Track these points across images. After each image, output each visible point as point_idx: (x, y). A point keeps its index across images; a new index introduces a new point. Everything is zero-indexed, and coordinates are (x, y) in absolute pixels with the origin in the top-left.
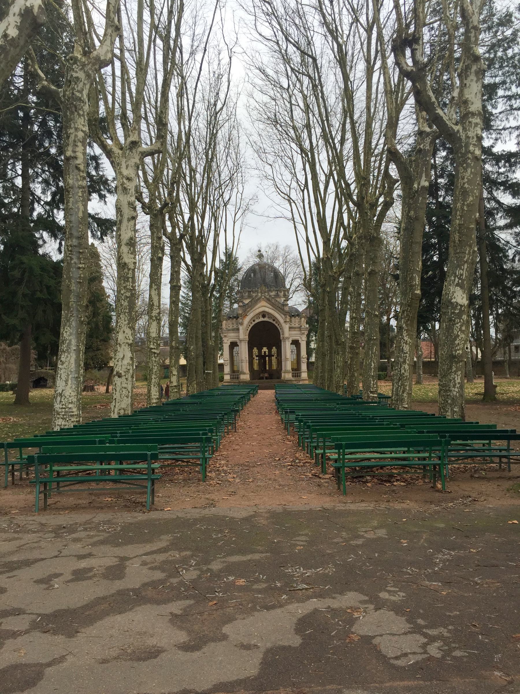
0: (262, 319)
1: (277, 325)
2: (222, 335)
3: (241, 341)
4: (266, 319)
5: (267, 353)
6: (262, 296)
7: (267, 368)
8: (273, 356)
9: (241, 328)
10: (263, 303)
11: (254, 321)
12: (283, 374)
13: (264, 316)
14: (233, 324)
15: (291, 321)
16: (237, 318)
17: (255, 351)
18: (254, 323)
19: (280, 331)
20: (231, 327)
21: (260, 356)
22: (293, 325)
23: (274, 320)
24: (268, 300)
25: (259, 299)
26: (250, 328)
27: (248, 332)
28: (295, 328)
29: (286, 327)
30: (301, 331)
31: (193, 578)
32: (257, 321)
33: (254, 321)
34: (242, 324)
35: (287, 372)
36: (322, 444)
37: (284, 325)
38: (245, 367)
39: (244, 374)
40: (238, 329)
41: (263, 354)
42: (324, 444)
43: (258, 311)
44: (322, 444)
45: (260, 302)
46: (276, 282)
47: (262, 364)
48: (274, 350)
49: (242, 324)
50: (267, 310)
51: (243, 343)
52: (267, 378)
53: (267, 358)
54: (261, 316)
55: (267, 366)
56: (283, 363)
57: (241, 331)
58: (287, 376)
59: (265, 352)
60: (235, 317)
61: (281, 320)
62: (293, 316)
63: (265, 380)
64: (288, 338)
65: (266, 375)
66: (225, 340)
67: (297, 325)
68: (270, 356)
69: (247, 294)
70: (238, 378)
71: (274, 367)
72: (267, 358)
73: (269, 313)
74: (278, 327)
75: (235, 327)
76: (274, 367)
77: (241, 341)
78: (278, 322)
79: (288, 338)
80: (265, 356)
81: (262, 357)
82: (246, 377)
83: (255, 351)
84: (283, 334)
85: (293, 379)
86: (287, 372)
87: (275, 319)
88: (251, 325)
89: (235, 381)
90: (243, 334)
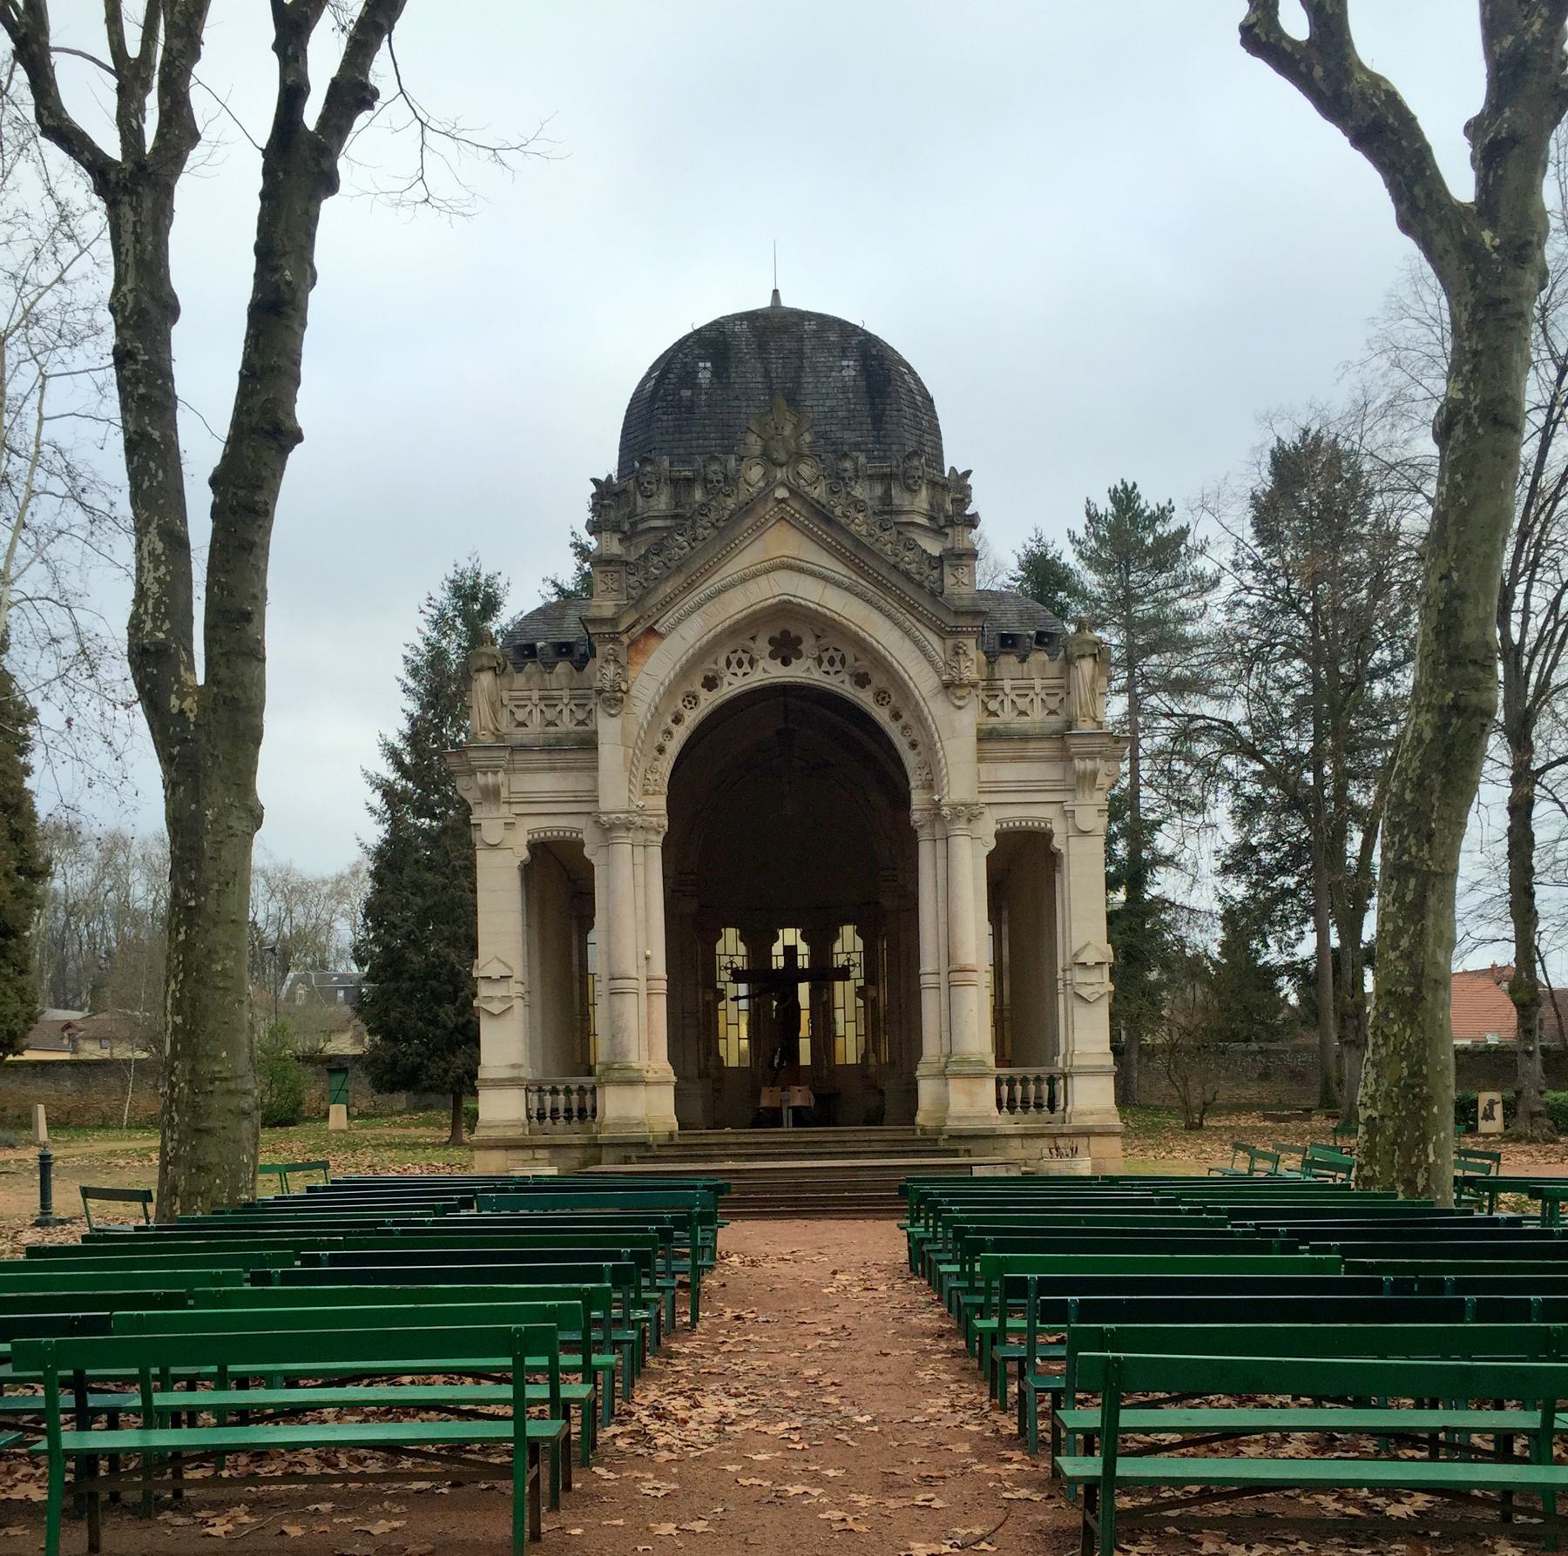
0: (769, 672)
1: (881, 715)
2: (466, 788)
3: (608, 830)
4: (801, 672)
5: (803, 962)
6: (770, 485)
7: (805, 1059)
8: (844, 974)
9: (608, 729)
10: (782, 542)
11: (711, 683)
12: (927, 1090)
13: (786, 649)
14: (549, 701)
15: (991, 687)
16: (575, 654)
17: (731, 947)
18: (709, 701)
19: (910, 759)
20: (535, 728)
21: (759, 976)
22: (1007, 717)
23: (862, 680)
24: (822, 521)
25: (746, 509)
26: (681, 733)
27: (666, 765)
28: (1025, 737)
29: (955, 729)
30: (1066, 757)
31: (1055, 842)
32: (734, 684)
33: (711, 683)
34: (615, 699)
35: (954, 1069)
36: (543, 1392)
37: (937, 709)
38: (637, 1025)
39: (633, 1081)
40: (588, 744)
41: (779, 963)
42: (519, 1392)
43: (738, 604)
44: (532, 1392)
45: (760, 529)
46: (878, 421)
47: (774, 1030)
48: (848, 944)
49: (615, 699)
50: (810, 593)
51: (623, 849)
52: (801, 1118)
53: (804, 989)
54: (762, 646)
55: (805, 1046)
56: (930, 1005)
57: (611, 754)
58: (959, 1098)
59: (790, 952)
60: (563, 650)
61: (921, 677)
62: (1009, 642)
63: (787, 1132)
64: (971, 813)
65: (800, 1097)
66: (489, 824)
67: (1037, 717)
68: (824, 974)
69: (662, 502)
70: (585, 1114)
71: (849, 1046)
72: (804, 989)
73: (825, 626)
74: (893, 729)
75: (567, 725)
76: (849, 1046)
77: (608, 830)
78: (894, 689)
79: (971, 813)
80: (792, 974)
81: (772, 987)
82: (645, 1104)
83: (731, 947)
84: (930, 786)
85: (1003, 1122)
86: (954, 1069)
87: (870, 666)
88: (692, 718)
89: (563, 1133)
90: (629, 780)
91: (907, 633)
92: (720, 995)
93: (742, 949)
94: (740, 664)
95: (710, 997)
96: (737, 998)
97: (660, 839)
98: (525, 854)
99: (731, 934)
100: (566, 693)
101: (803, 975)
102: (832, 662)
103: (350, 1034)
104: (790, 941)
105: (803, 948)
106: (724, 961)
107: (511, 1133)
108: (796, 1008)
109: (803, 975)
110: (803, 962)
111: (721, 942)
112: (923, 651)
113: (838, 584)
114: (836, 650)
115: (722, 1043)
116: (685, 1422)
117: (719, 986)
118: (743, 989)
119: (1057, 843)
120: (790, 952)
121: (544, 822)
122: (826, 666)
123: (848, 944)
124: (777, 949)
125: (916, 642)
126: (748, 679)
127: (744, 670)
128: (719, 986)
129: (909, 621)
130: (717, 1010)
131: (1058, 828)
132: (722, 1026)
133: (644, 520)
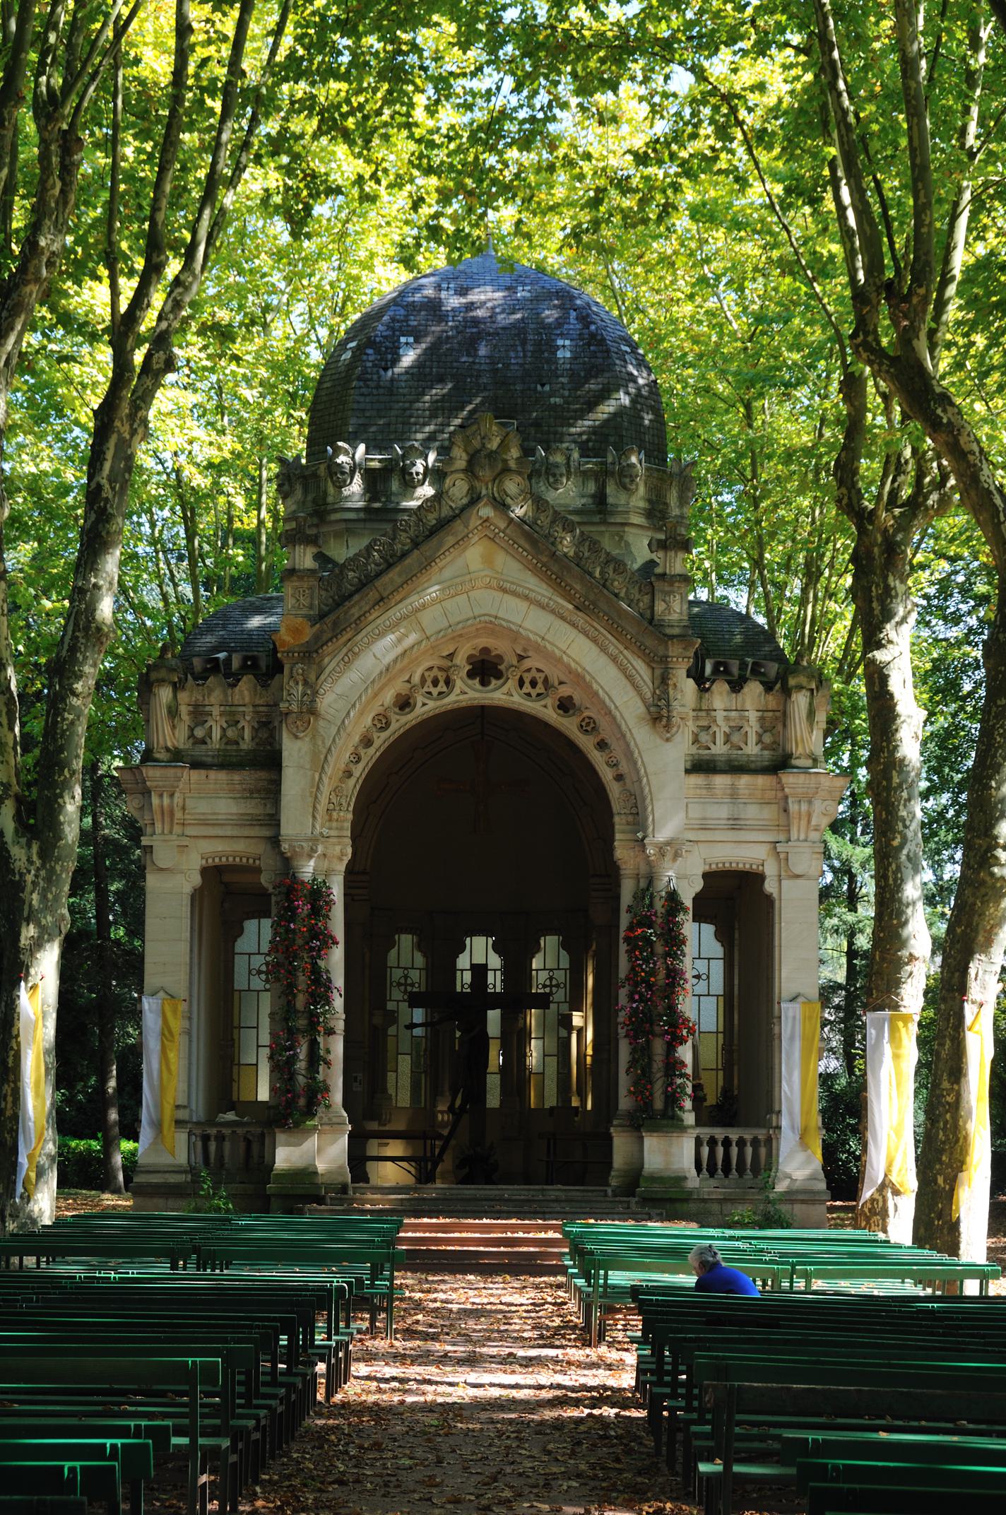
5: (495, 981)
17: (406, 957)
29: (662, 763)
37: (641, 736)
50: (515, 612)
53: (494, 1016)
59: (479, 971)
72: (494, 1016)
80: (480, 997)
83: (406, 957)
91: (614, 659)
92: (392, 1017)
93: (420, 960)
94: (435, 683)
95: (377, 1020)
96: (412, 1026)
97: (343, 868)
98: (197, 880)
99: (406, 941)
100: (249, 709)
101: (495, 1001)
102: (534, 684)
103: (781, 1187)
104: (479, 959)
105: (495, 961)
106: (397, 974)
107: (173, 1179)
108: (484, 1039)
109: (495, 1001)
110: (495, 981)
111: (393, 953)
112: (629, 678)
113: (543, 607)
114: (539, 670)
115: (391, 1076)
116: (750, 426)
117: (391, 1006)
118: (419, 1015)
119: (770, 886)
120: (479, 971)
121: (219, 846)
122: (527, 688)
123: (546, 962)
124: (463, 961)
125: (623, 670)
126: (447, 700)
127: (439, 689)
128: (391, 1006)
129: (614, 646)
130: (386, 1035)
131: (770, 870)
132: (391, 1054)
133: (336, 511)
